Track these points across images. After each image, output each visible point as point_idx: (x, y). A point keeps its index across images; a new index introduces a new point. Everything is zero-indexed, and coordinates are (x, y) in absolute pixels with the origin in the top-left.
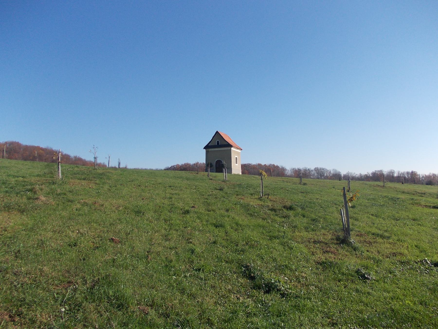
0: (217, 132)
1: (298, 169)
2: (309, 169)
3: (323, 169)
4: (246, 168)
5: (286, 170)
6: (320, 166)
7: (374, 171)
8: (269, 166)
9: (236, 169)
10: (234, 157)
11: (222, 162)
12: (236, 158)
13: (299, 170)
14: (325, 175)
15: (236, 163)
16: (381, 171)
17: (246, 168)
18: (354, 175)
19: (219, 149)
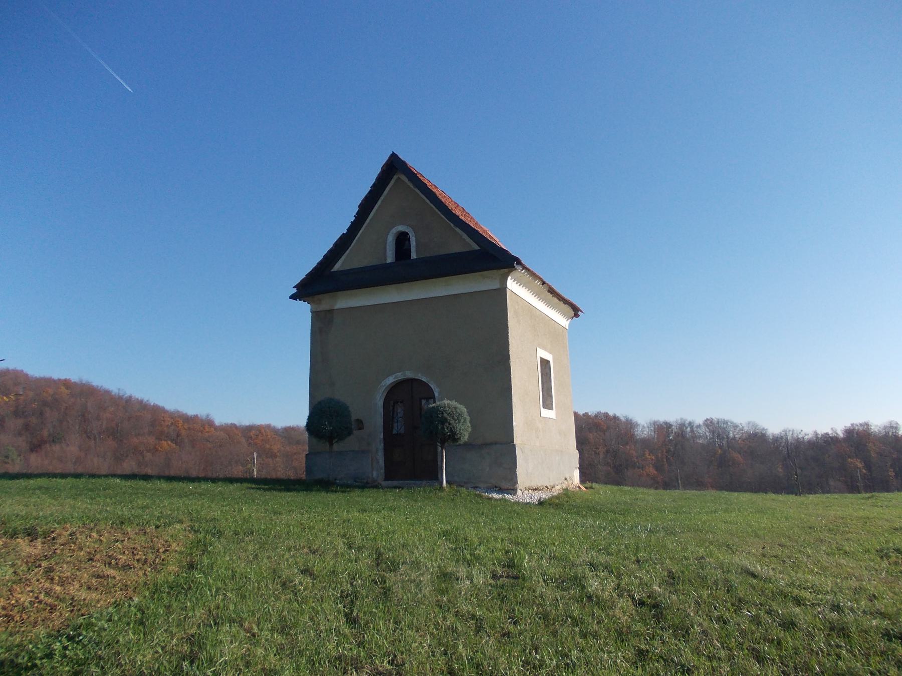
0: (394, 167)
1: (666, 423)
2: (690, 423)
3: (726, 422)
4: (604, 445)
5: (637, 425)
6: (717, 414)
7: (848, 425)
8: (596, 416)
9: (545, 457)
10: (525, 353)
11: (431, 397)
12: (545, 363)
13: (668, 425)
14: (731, 435)
15: (548, 405)
16: (867, 424)
17: (604, 445)
18: (800, 436)
19: (409, 291)
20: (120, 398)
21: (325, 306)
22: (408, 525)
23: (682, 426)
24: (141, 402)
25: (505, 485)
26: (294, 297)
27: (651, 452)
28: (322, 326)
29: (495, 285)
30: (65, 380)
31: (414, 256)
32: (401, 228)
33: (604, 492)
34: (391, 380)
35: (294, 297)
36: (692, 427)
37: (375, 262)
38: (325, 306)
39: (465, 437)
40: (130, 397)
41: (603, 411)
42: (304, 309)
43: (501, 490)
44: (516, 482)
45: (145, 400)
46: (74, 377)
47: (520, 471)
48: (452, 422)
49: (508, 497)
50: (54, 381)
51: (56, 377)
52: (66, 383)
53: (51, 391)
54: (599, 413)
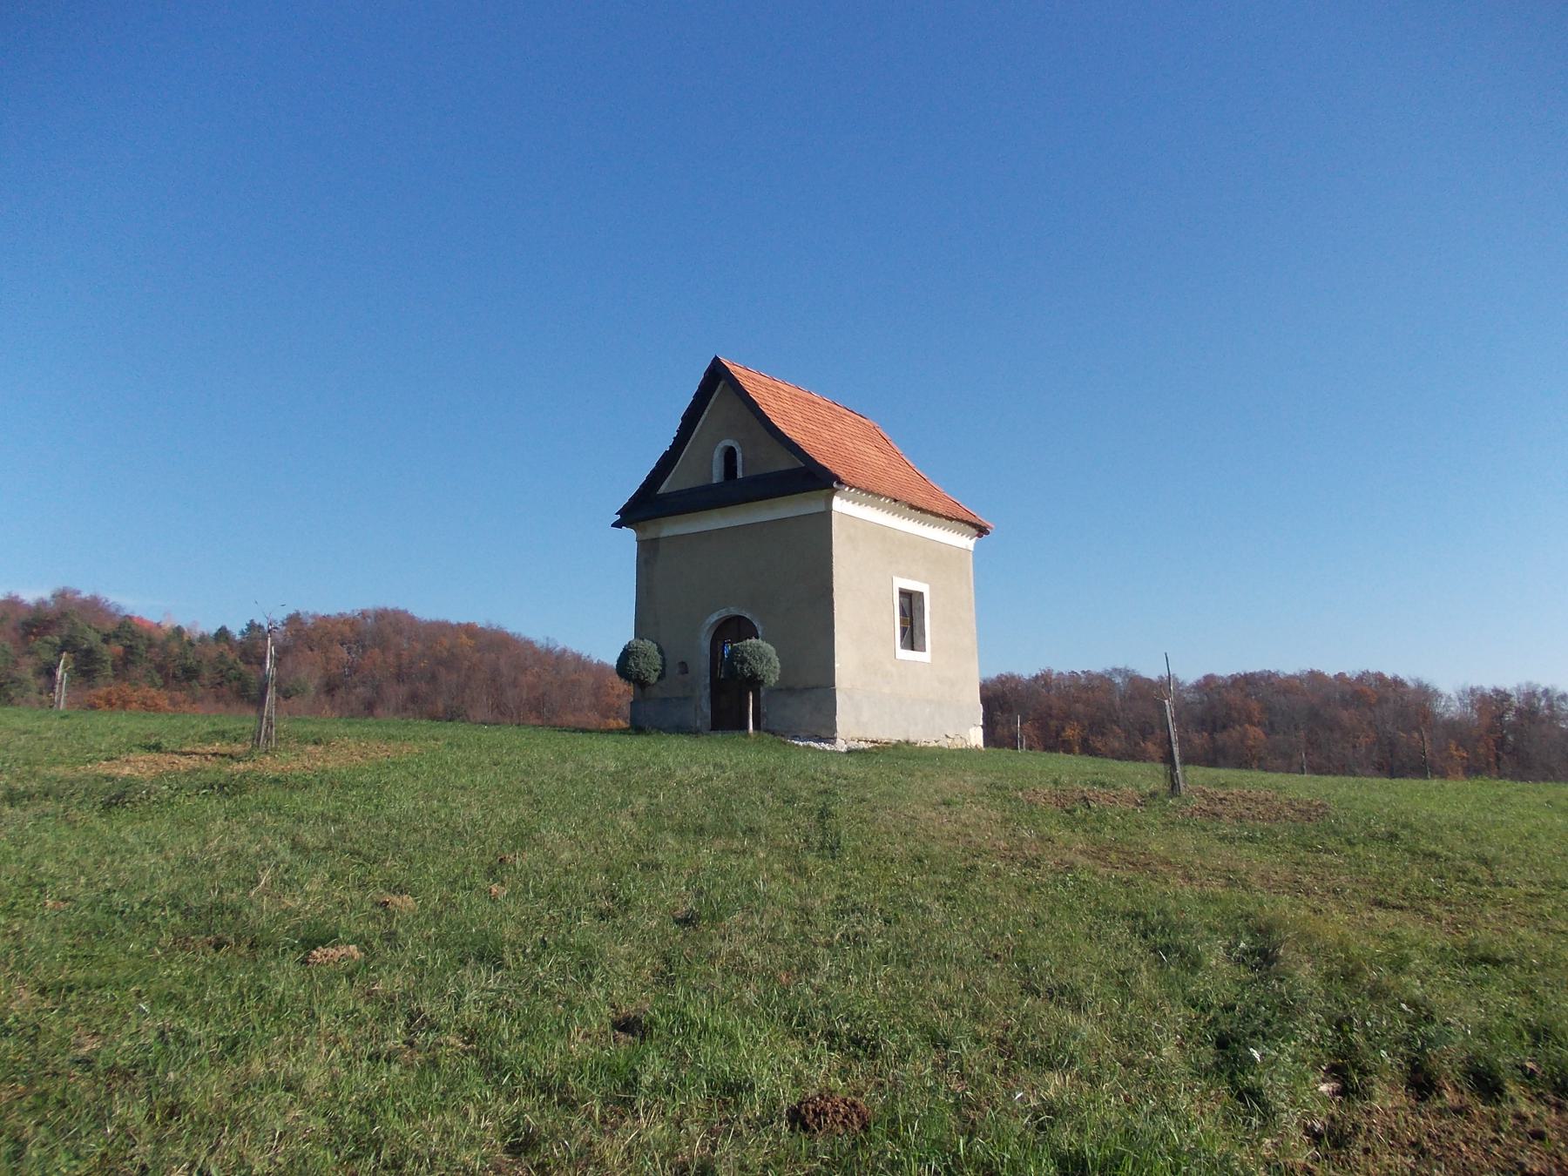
0: (717, 374)
1: (1497, 691)
2: (1546, 692)
5: (1436, 694)
8: (1360, 679)
13: (1502, 697)
20: (549, 652)
21: (651, 533)
22: (693, 763)
23: (1531, 695)
24: (578, 658)
25: (824, 734)
26: (617, 525)
27: (1461, 744)
28: (648, 554)
29: (821, 508)
30: (468, 625)
31: (740, 475)
32: (729, 442)
33: (991, 750)
34: (714, 618)
35: (617, 525)
36: (1549, 699)
37: (701, 483)
38: (651, 533)
39: (773, 679)
40: (565, 651)
41: (1373, 670)
42: (629, 535)
43: (820, 740)
44: (835, 731)
45: (585, 655)
46: (481, 616)
47: (841, 718)
48: (753, 662)
49: (827, 747)
50: (452, 626)
51: (454, 620)
52: (470, 630)
53: (447, 642)
54: (1366, 673)
